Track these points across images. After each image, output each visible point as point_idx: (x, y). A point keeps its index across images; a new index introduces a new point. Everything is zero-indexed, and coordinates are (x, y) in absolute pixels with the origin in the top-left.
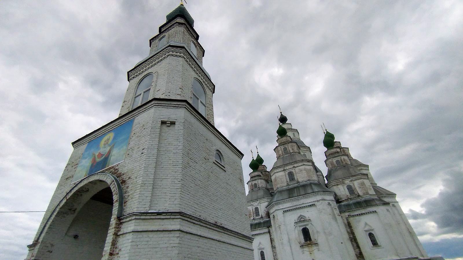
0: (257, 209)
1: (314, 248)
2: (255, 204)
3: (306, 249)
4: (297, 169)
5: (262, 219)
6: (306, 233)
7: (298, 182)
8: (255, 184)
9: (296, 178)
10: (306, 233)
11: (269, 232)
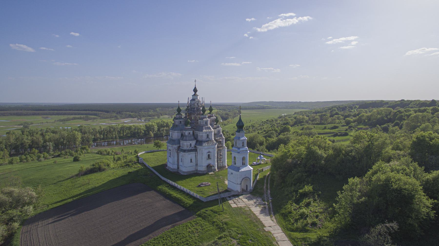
0: (191, 144)
1: (210, 160)
2: (191, 142)
3: (208, 160)
4: (210, 134)
5: (227, 193)
6: (209, 155)
7: (209, 139)
8: (189, 133)
9: (209, 137)
10: (209, 155)
11: (195, 153)
